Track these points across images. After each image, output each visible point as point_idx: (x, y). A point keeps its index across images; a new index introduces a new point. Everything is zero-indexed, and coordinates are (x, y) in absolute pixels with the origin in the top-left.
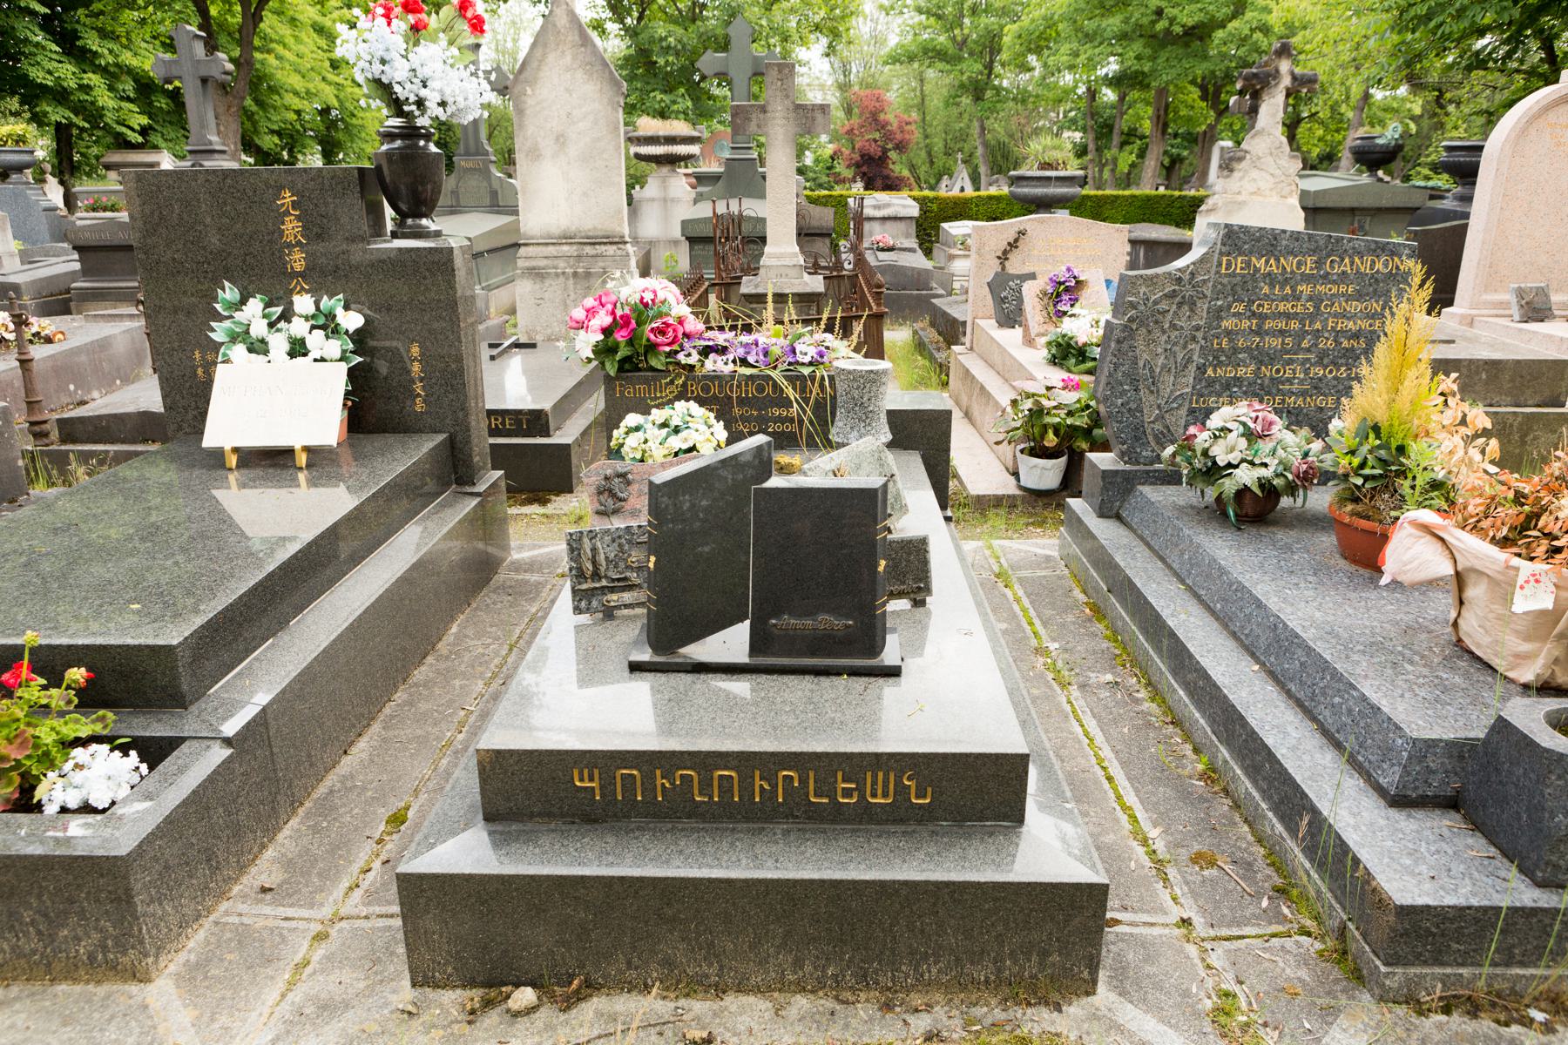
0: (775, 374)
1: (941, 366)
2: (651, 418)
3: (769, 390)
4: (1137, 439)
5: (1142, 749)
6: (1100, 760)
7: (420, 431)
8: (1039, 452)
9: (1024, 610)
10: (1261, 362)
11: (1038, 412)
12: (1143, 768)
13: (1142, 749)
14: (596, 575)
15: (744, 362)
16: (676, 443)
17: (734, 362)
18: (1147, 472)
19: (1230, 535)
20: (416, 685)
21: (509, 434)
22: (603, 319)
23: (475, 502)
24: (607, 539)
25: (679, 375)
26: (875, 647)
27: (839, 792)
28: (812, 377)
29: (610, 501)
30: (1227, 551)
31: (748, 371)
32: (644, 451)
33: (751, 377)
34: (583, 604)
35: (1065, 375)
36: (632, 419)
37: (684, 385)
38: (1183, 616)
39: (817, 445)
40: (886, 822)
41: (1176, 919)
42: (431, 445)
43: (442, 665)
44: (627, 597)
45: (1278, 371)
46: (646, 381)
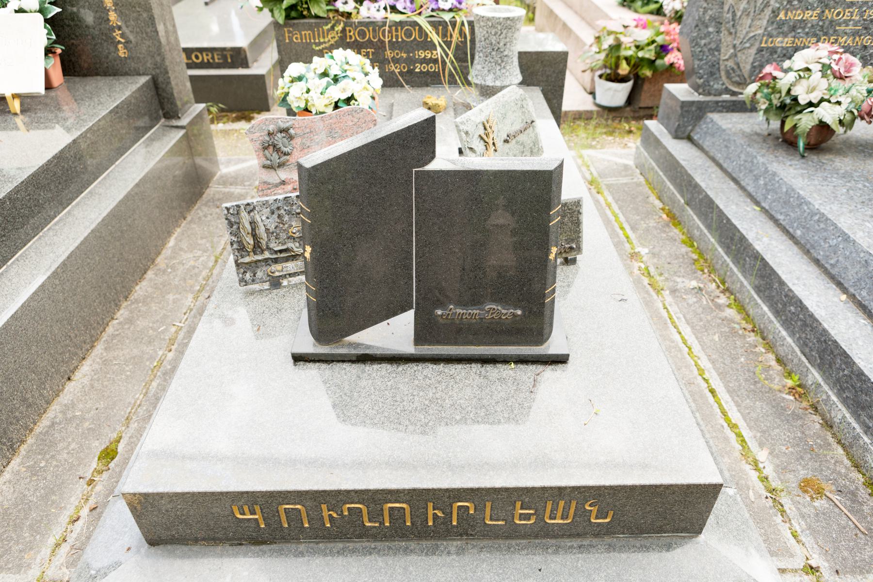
0: (422, 21)
1: (528, 6)
2: (312, 66)
3: (415, 35)
4: (712, 74)
5: (734, 359)
6: (701, 372)
7: (126, 74)
8: (615, 78)
9: (616, 216)
10: (827, 6)
11: (617, 46)
12: (737, 380)
13: (734, 359)
14: (257, 247)
16: (338, 93)
17: (385, 8)
18: (717, 102)
19: (797, 162)
20: (137, 301)
21: (218, 66)
23: (182, 132)
24: (266, 211)
25: (338, 22)
26: (540, 335)
27: (517, 516)
28: (454, 24)
29: (275, 155)
30: (792, 173)
31: (397, 18)
32: (307, 101)
33: (401, 24)
34: (248, 276)
35: (636, 16)
36: (295, 69)
37: (344, 30)
38: (765, 239)
39: (456, 83)
40: (562, 536)
41: (799, 563)
42: (134, 87)
43: (160, 280)
44: (291, 266)
45: (838, 14)
46: (310, 27)
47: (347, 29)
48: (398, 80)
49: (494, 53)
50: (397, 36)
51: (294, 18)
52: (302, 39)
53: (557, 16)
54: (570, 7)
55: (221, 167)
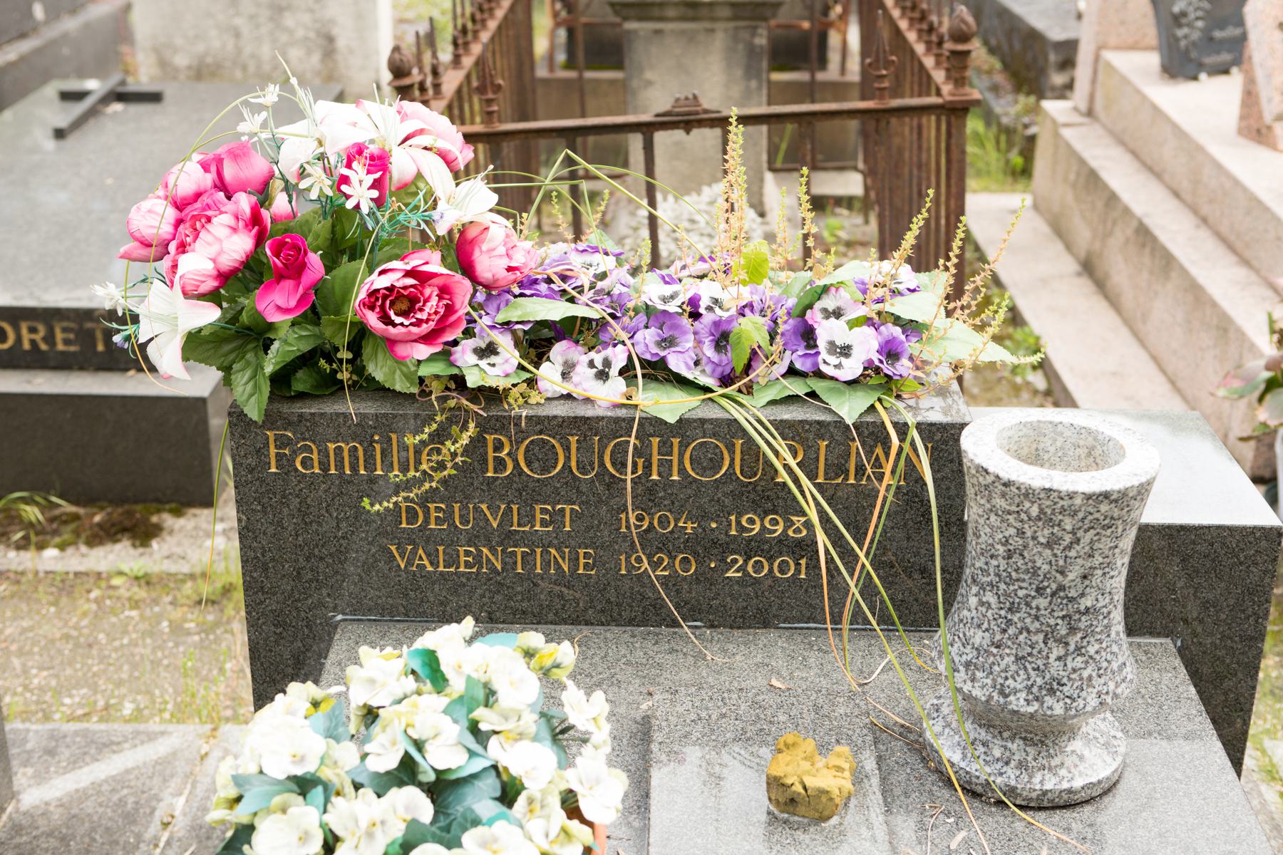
15: (657, 372)
21: (63, 364)
22: (223, 243)
25: (458, 418)
47: (490, 438)
48: (658, 605)
49: (1042, 602)
50: (665, 466)
51: (302, 396)
52: (325, 467)
53: (1112, 198)
54: (1154, 171)
55: (22, 777)
